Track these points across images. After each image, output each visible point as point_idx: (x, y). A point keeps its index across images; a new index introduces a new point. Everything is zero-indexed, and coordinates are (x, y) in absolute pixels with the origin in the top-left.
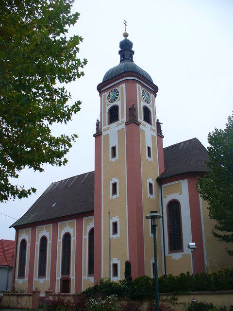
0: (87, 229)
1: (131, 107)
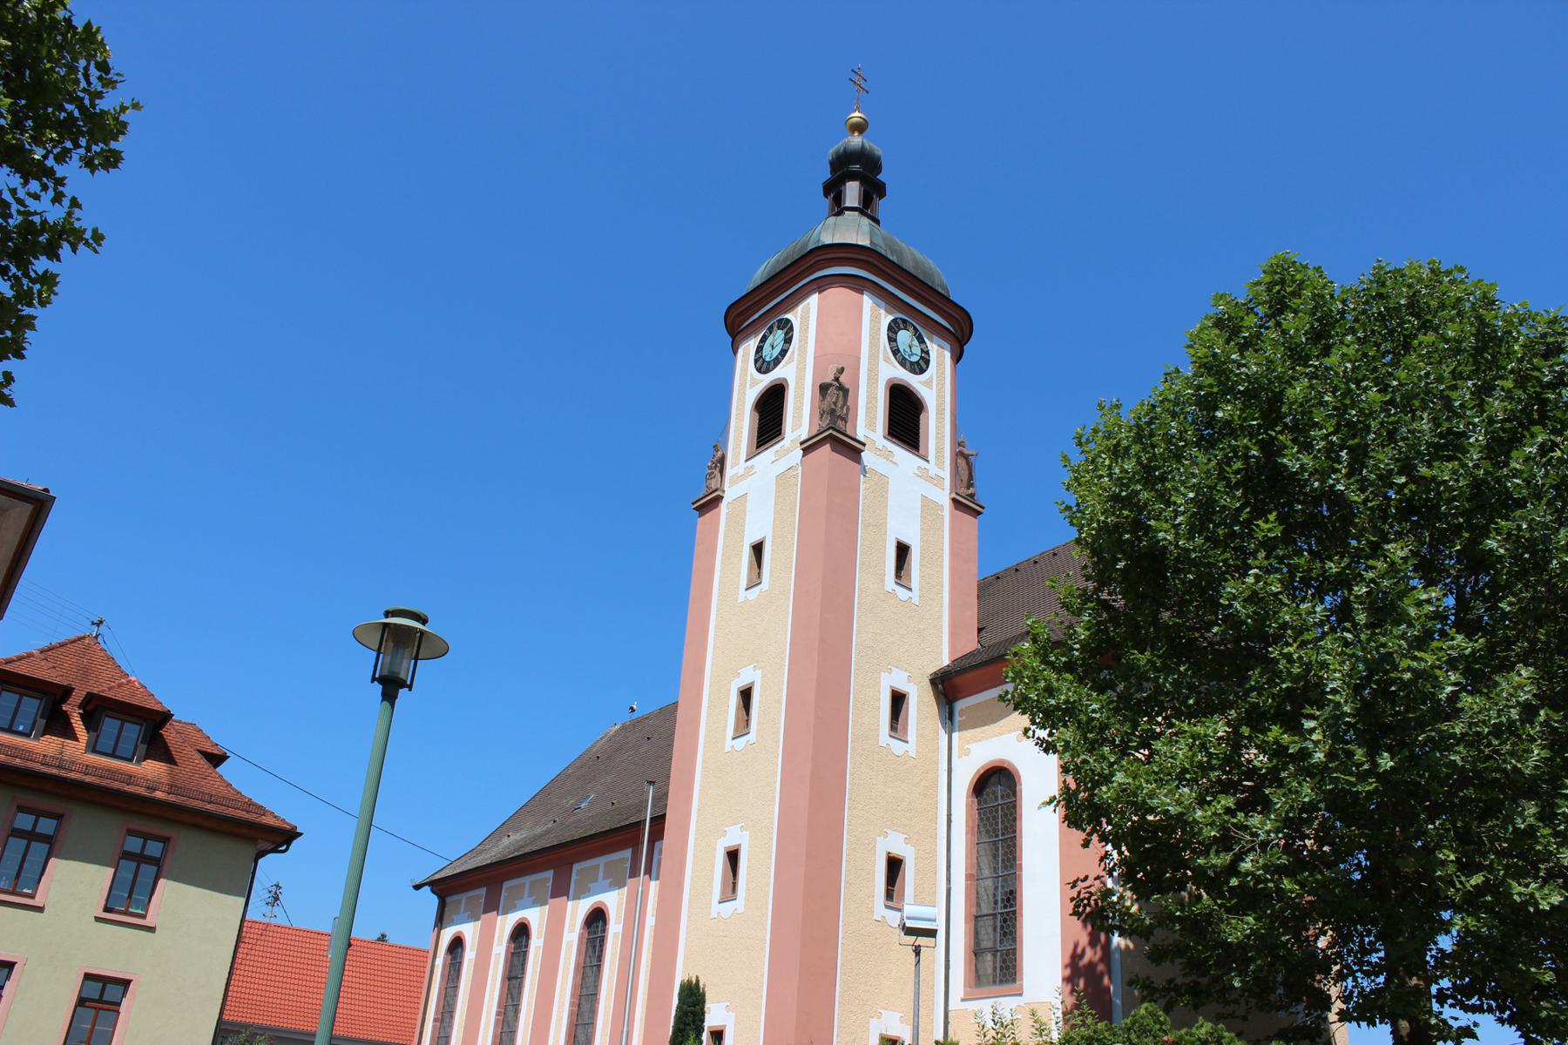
0: (507, 926)
1: (829, 379)
